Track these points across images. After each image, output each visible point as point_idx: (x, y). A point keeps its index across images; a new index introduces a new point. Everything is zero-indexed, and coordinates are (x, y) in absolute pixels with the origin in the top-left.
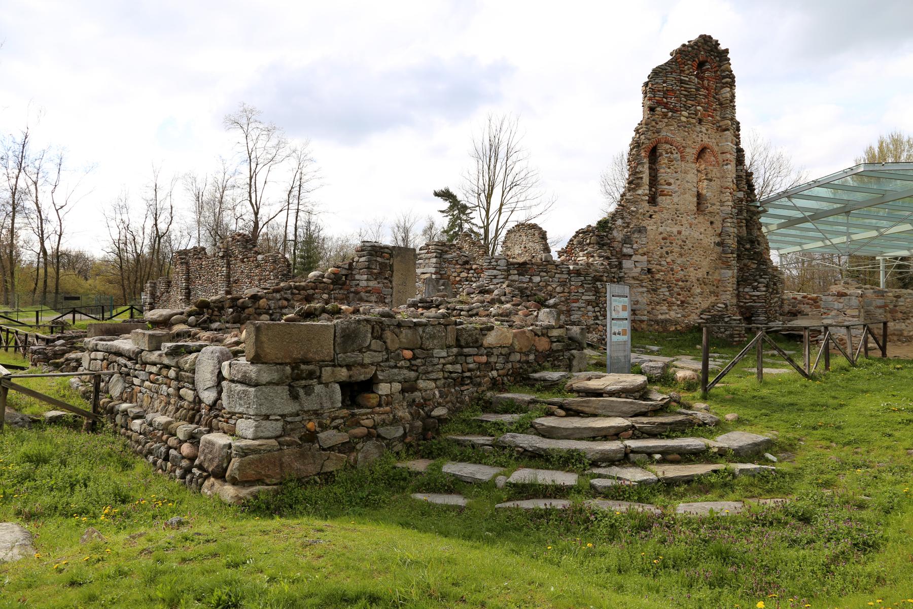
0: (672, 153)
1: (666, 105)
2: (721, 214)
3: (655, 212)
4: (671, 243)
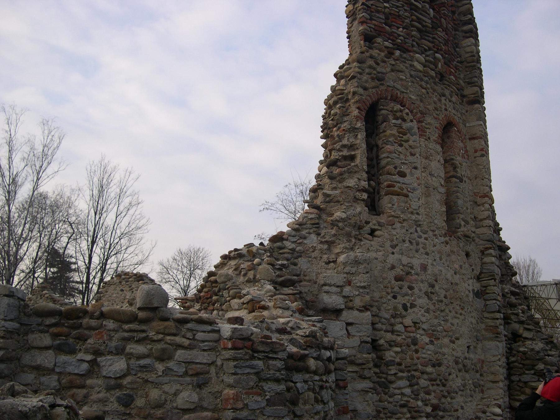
0: (404, 120)
1: (391, 37)
2: (477, 240)
3: (379, 224)
4: (411, 288)
